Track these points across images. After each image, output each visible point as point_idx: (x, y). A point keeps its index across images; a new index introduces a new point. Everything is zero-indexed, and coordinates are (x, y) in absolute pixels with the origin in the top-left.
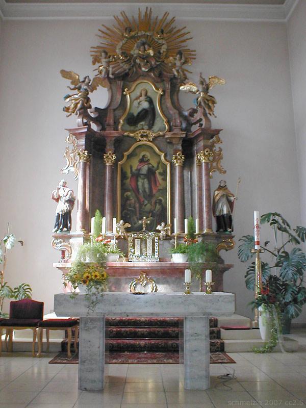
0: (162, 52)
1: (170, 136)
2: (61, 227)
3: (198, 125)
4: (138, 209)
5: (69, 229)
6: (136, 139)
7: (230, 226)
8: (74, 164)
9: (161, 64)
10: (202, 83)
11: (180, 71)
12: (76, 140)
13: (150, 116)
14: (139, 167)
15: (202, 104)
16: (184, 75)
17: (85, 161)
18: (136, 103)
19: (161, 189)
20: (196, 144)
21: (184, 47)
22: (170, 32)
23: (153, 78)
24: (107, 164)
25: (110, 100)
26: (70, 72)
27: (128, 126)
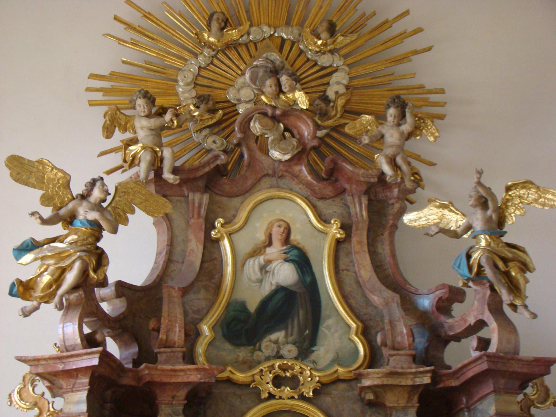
0: (331, 93)
1: (376, 382)
3: (473, 342)
6: (258, 393)
9: (328, 135)
10: (483, 203)
11: (399, 160)
12: (48, 395)
13: (301, 313)
15: (488, 272)
16: (415, 173)
20: (468, 408)
21: (403, 77)
23: (308, 185)
26: (40, 162)
27: (228, 346)
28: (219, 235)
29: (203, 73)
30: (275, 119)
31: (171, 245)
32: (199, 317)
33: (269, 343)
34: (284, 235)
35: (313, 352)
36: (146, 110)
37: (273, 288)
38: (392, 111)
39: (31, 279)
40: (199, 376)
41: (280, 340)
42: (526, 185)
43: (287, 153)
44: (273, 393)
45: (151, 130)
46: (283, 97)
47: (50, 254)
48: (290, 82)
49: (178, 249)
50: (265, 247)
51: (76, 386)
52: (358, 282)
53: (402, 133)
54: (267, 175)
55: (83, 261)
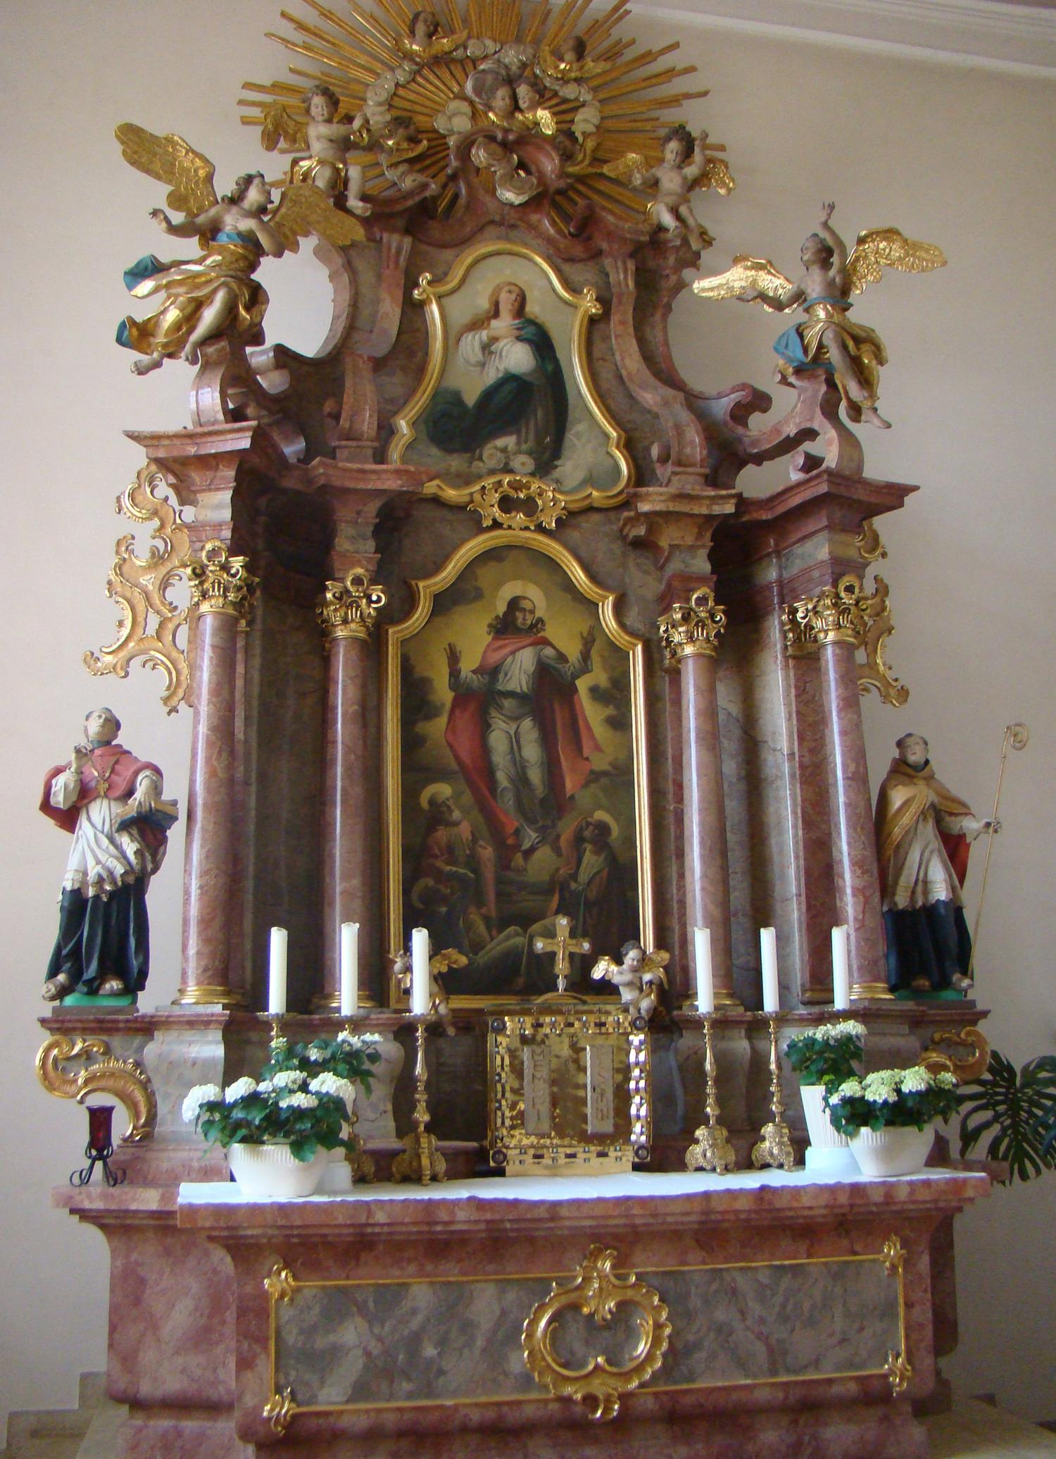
1: (658, 507)
2: (92, 970)
4: (489, 874)
5: (135, 983)
7: (964, 966)
8: (162, 625)
9: (571, 187)
12: (173, 500)
13: (540, 413)
14: (494, 658)
17: (231, 611)
18: (471, 345)
19: (605, 774)
20: (778, 553)
22: (612, 54)
23: (550, 241)
24: (340, 633)
25: (342, 323)
26: (169, 140)
27: (434, 451)
28: (425, 296)
29: (401, 92)
30: (504, 145)
31: (355, 305)
32: (395, 409)
33: (492, 451)
34: (516, 304)
35: (556, 467)
36: (325, 113)
37: (501, 375)
38: (674, 146)
39: (149, 319)
40: (399, 482)
41: (509, 449)
42: (889, 235)
43: (524, 193)
44: (500, 520)
45: (331, 141)
46: (519, 116)
47: (179, 278)
48: (531, 94)
49: (365, 312)
50: (489, 319)
51: (216, 482)
52: (620, 378)
53: (685, 178)
54: (492, 222)
55: (230, 290)
